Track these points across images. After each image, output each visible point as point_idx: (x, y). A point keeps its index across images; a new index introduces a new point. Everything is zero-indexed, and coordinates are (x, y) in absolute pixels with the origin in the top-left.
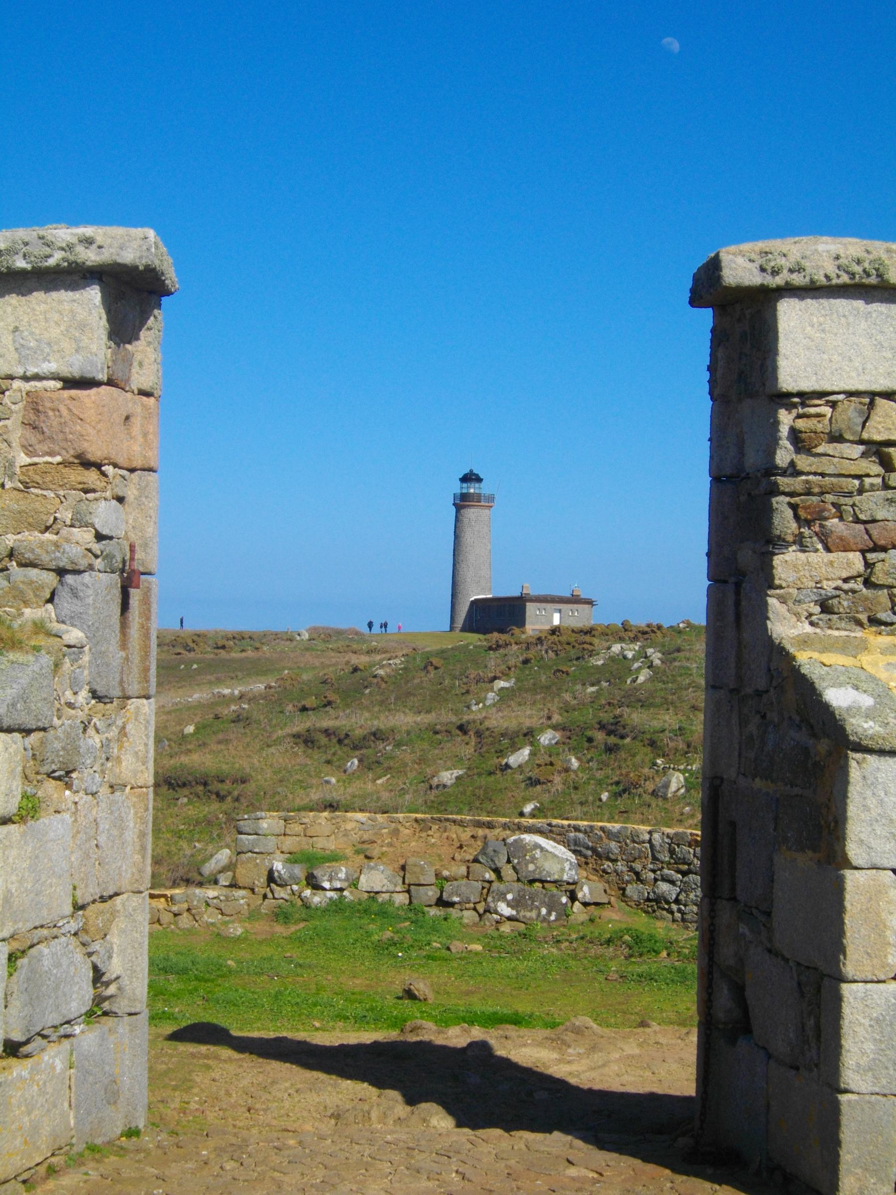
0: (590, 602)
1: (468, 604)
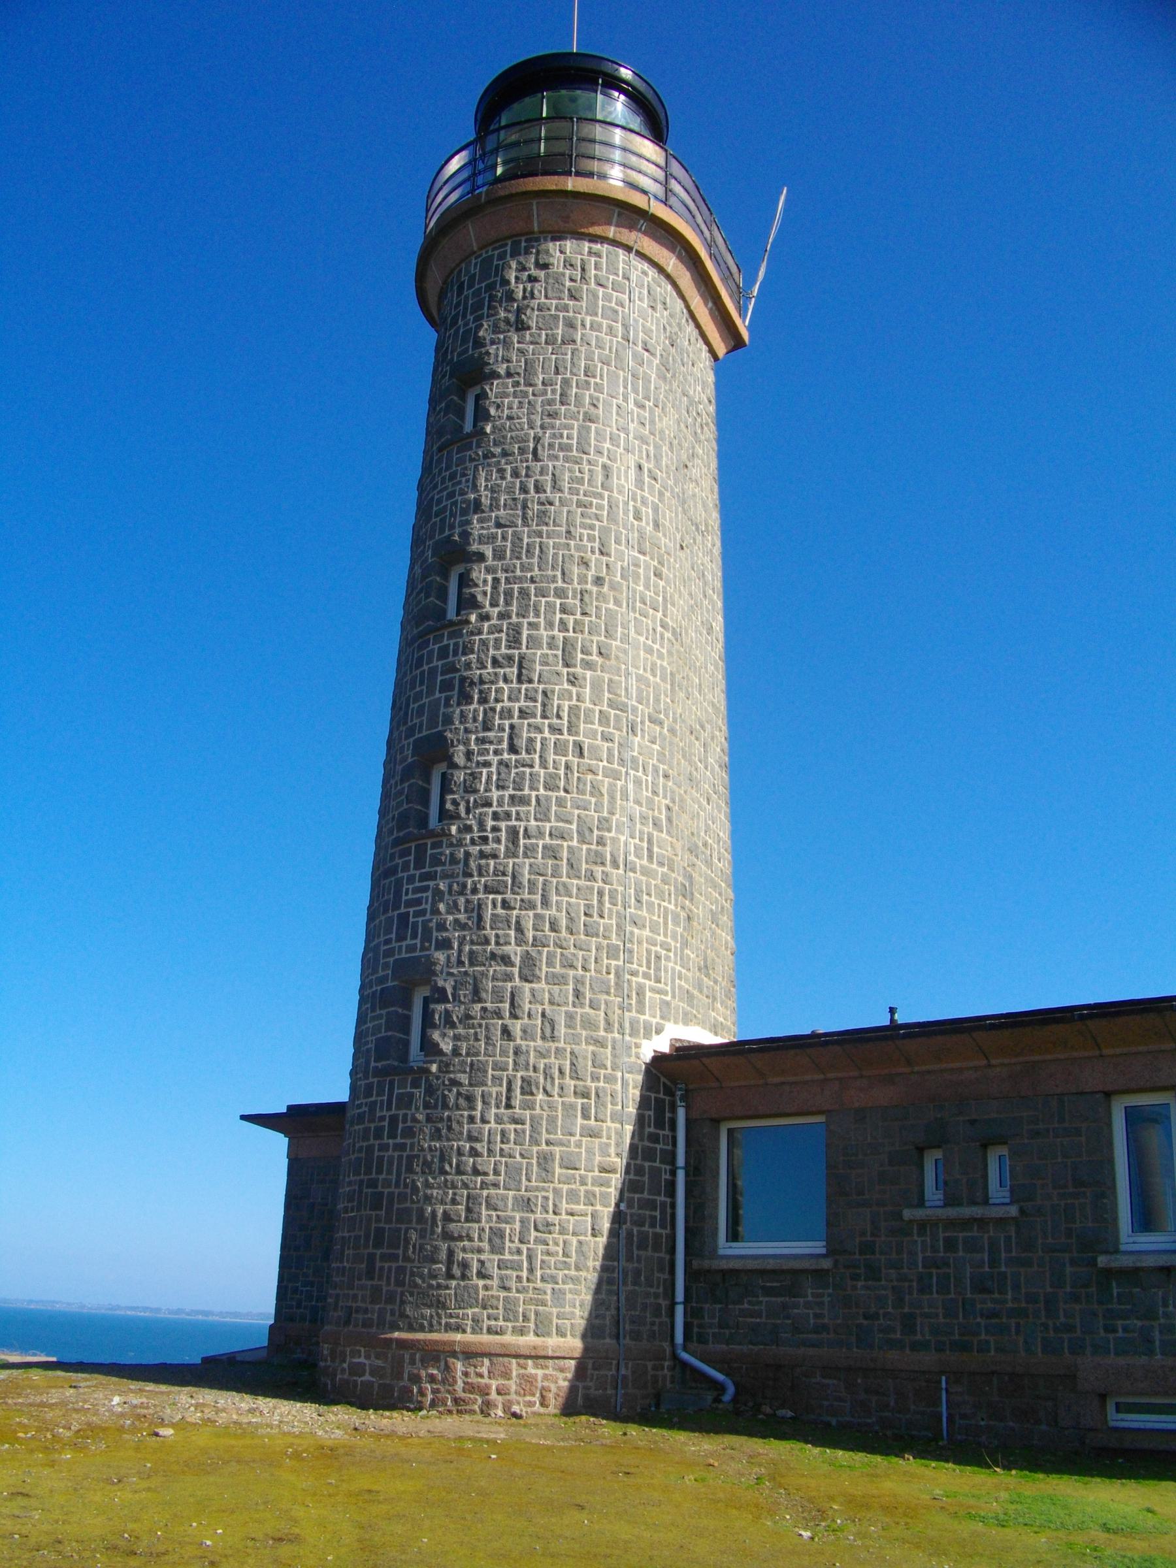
0: (243, 1117)
1: (627, 1091)
